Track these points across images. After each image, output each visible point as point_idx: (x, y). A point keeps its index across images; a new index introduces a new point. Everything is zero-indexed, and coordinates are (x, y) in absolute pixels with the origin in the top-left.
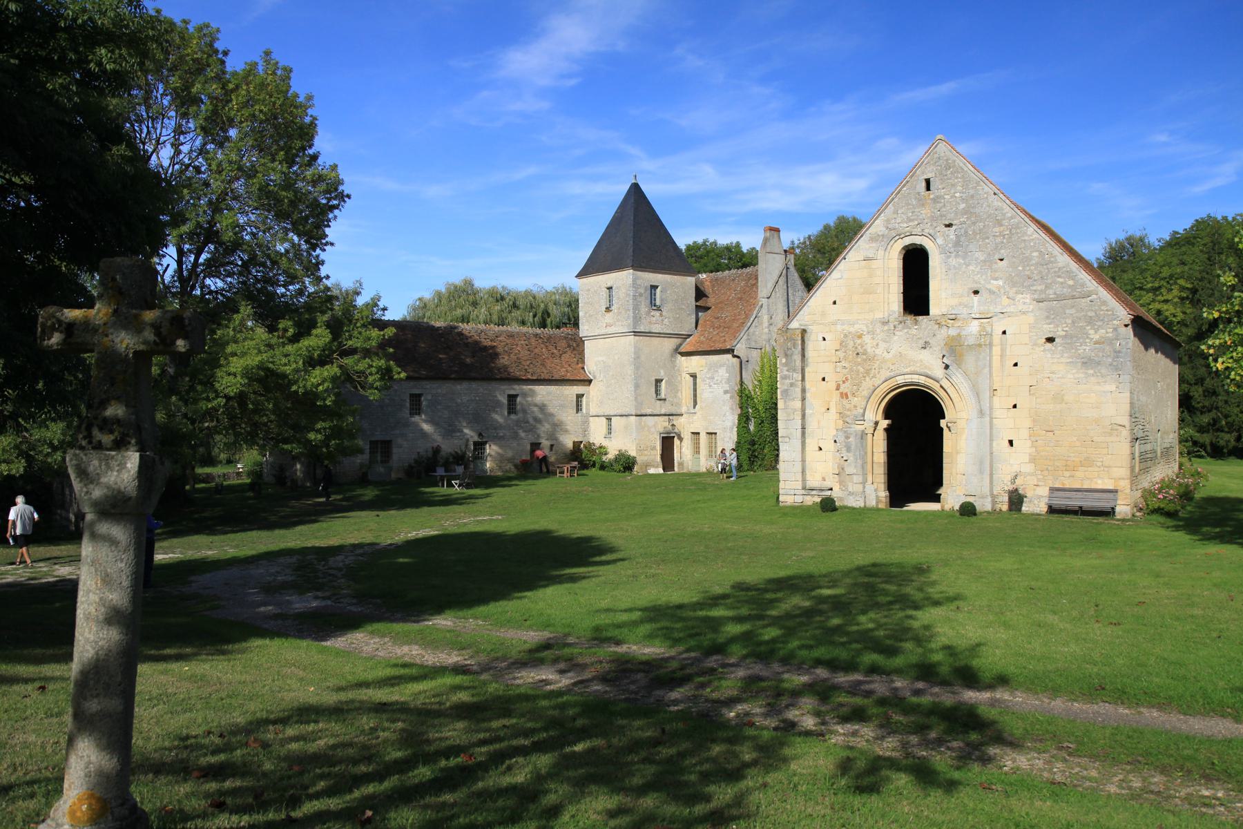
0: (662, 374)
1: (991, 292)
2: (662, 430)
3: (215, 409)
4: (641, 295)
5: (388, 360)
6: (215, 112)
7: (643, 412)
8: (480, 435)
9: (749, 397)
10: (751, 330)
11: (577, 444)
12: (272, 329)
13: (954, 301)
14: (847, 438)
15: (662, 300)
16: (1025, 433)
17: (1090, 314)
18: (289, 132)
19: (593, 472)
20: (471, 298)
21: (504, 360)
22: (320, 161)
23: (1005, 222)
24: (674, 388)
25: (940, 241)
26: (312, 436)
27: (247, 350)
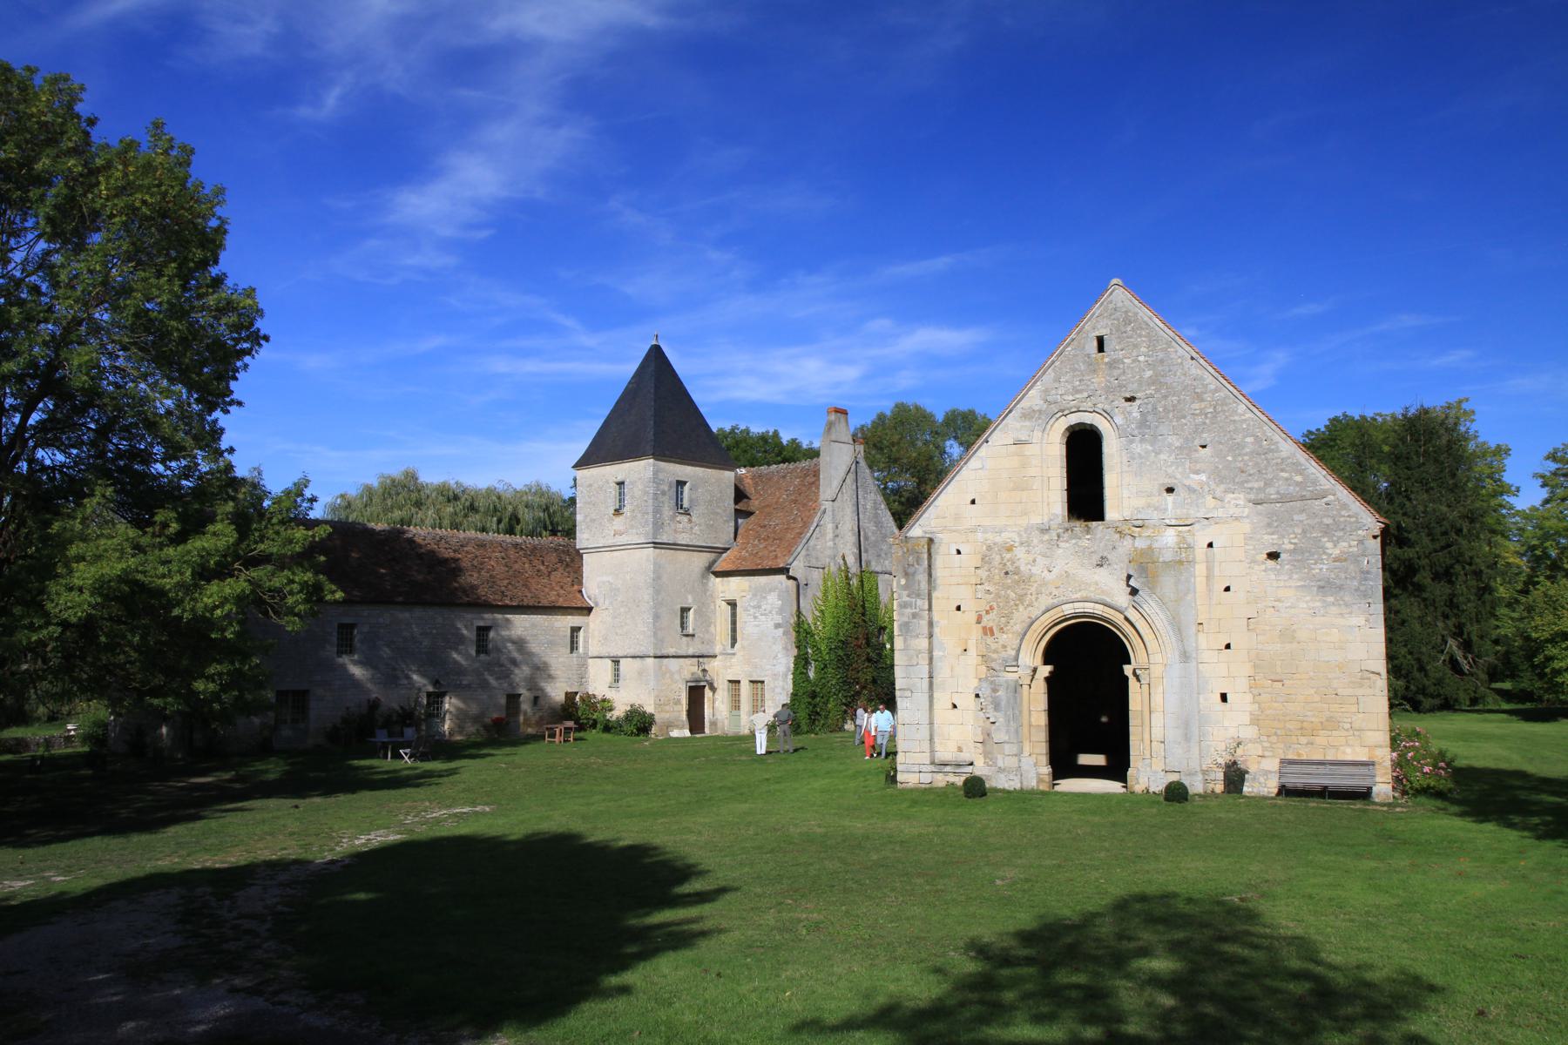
0: (689, 601)
1: (1191, 490)
2: (688, 677)
3: (42, 643)
4: (664, 493)
5: (316, 573)
6: (71, 199)
7: (664, 652)
8: (436, 683)
9: (809, 633)
10: (811, 543)
11: (570, 696)
12: (140, 524)
13: (1141, 502)
14: (995, 690)
15: (691, 501)
16: (1243, 684)
17: (1328, 521)
18: (182, 237)
19: (592, 735)
20: (414, 496)
21: (471, 578)
22: (229, 282)
23: (1208, 397)
24: (706, 620)
25: (1119, 420)
26: (199, 685)
27: (101, 554)
